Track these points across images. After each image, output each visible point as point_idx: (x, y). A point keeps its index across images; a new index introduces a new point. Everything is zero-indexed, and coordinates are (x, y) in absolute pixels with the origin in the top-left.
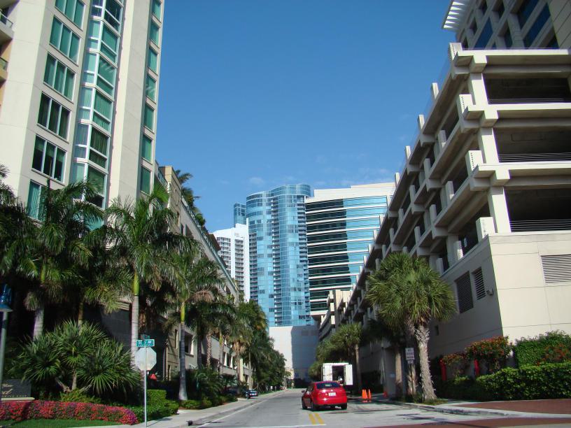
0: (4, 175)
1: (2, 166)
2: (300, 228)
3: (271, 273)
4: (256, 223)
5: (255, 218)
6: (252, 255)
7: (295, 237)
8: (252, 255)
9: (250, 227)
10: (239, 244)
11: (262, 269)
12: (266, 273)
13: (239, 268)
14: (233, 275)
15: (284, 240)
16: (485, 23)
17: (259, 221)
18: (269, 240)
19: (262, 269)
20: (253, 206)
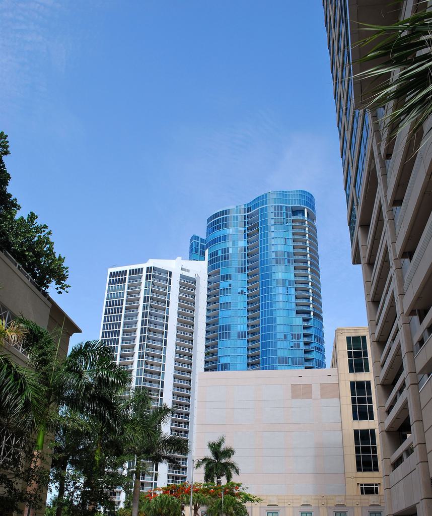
0: (5, 415)
1: (2, 133)
2: (297, 257)
3: (242, 335)
4: (220, 254)
5: (219, 247)
6: (210, 358)
7: (287, 271)
8: (210, 358)
9: (210, 262)
10: (189, 284)
11: (227, 328)
12: (234, 335)
13: (183, 379)
14: (168, 400)
15: (269, 276)
16: (405, 418)
17: (226, 250)
18: (239, 281)
19: (227, 328)
20: (219, 228)
